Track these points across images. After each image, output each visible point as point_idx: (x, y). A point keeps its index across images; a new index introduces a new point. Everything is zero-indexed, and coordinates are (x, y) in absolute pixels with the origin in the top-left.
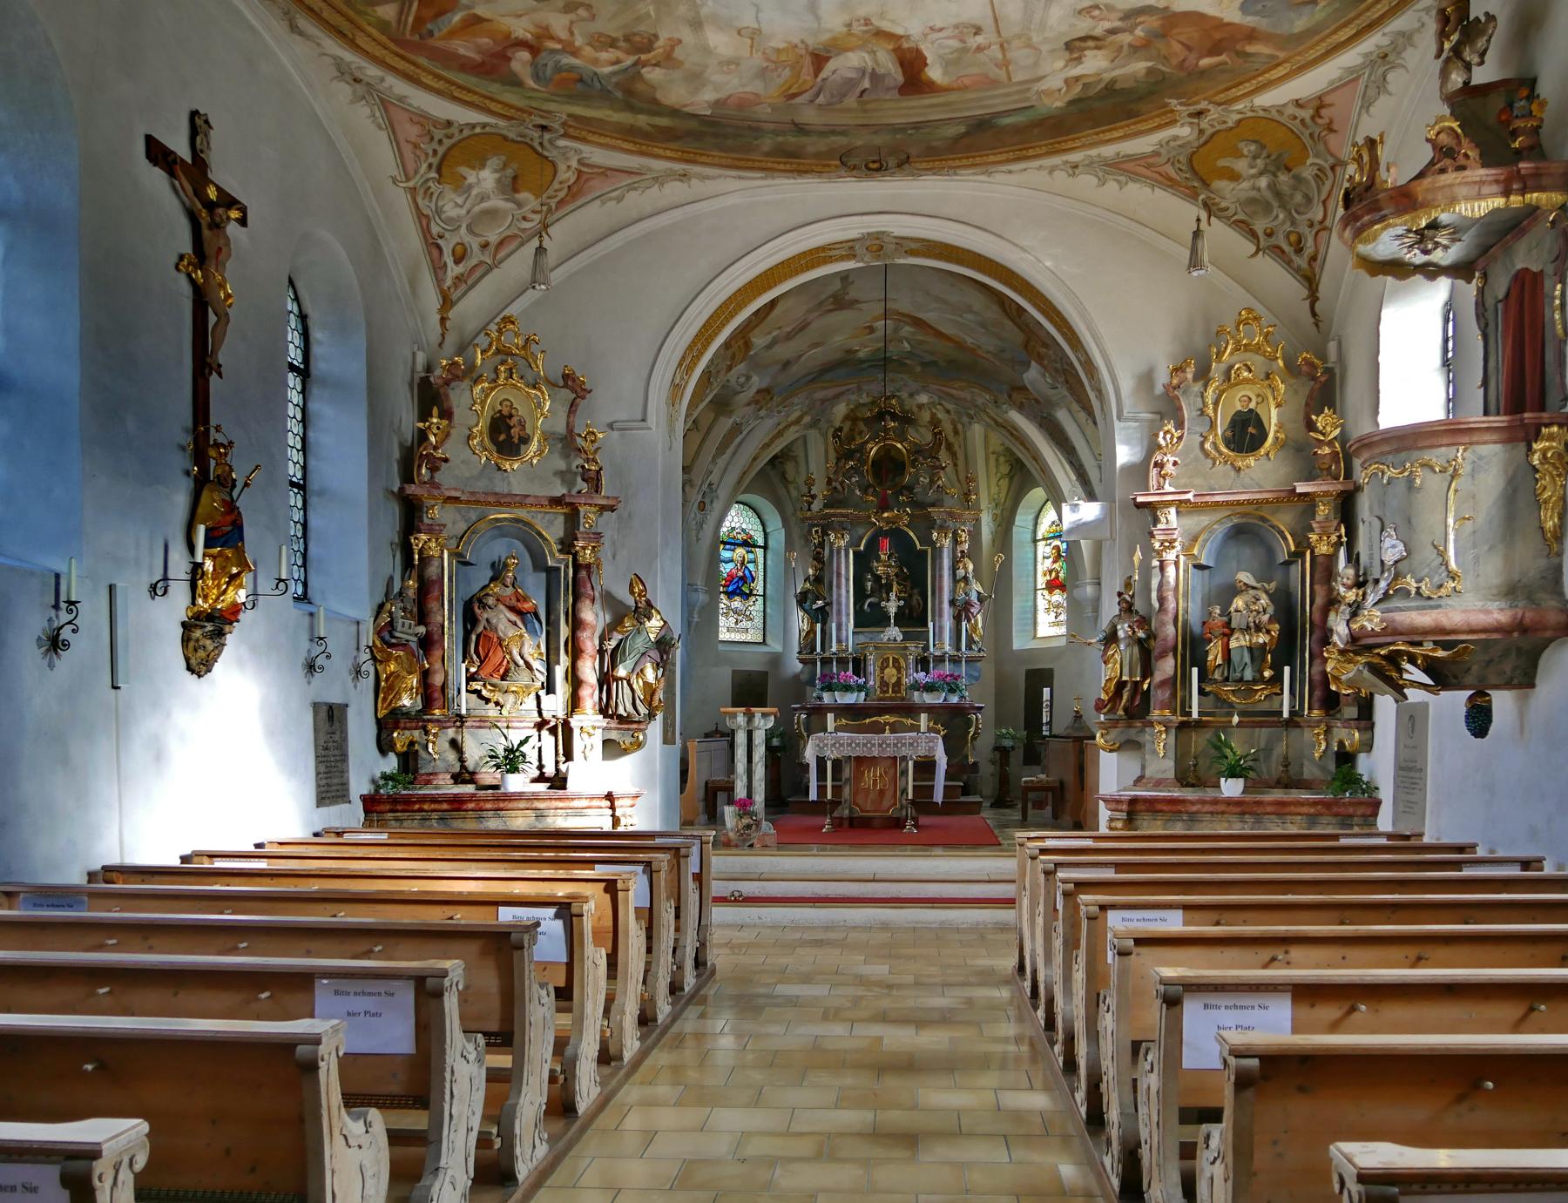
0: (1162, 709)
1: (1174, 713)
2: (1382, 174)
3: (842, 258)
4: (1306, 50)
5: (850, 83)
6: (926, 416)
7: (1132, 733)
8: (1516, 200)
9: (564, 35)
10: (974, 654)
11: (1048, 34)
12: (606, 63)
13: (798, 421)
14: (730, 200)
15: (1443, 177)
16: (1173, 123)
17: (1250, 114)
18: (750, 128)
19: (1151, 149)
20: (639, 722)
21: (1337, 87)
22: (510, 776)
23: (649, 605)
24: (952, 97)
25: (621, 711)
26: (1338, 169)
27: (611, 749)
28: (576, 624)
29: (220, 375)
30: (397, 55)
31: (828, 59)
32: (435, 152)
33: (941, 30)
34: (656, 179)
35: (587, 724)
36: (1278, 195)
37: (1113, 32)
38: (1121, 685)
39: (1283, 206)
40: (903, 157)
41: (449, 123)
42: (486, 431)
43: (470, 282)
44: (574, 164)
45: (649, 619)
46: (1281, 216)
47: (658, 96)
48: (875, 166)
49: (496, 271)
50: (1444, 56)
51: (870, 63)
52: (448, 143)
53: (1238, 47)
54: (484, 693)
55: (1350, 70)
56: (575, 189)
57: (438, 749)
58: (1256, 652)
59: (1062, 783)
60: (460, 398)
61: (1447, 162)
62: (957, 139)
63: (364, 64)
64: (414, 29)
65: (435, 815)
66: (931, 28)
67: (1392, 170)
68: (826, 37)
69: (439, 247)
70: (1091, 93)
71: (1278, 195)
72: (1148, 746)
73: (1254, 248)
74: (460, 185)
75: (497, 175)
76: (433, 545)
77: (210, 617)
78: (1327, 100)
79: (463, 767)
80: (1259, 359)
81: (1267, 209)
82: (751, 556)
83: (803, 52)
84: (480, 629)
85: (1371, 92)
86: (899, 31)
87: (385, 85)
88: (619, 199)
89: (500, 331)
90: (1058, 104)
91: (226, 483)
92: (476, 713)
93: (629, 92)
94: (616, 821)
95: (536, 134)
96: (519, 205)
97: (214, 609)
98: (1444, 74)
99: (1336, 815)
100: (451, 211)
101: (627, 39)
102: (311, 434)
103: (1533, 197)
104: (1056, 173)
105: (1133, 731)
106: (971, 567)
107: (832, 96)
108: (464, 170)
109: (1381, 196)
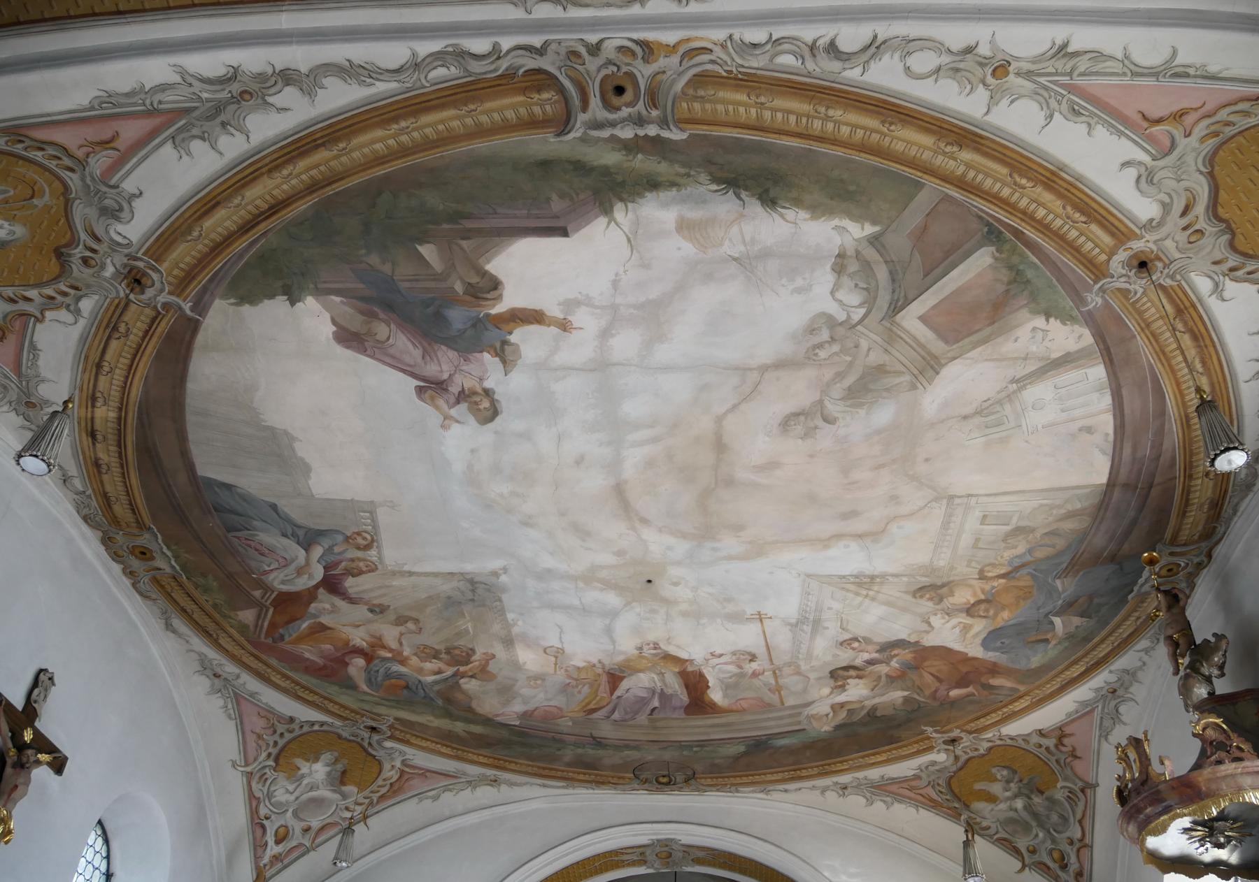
2: (1156, 767)
3: (633, 864)
4: (1043, 685)
5: (643, 701)
9: (394, 645)
11: (814, 663)
12: (430, 672)
14: (534, 805)
15: (1222, 767)
16: (929, 749)
17: (999, 742)
18: (554, 739)
19: (913, 772)
21: (1074, 718)
24: (732, 718)
26: (1088, 791)
30: (252, 655)
31: (622, 679)
32: (276, 743)
33: (721, 655)
34: (469, 782)
36: (1035, 815)
37: (871, 662)
39: (1041, 825)
40: (690, 773)
41: (292, 720)
43: (286, 861)
44: (398, 764)
46: (1041, 835)
47: (474, 705)
48: (665, 780)
49: (312, 853)
50: (1182, 673)
51: (659, 684)
52: (288, 736)
53: (983, 680)
55: (1084, 704)
56: (396, 787)
61: (1223, 754)
62: (737, 758)
63: (224, 661)
64: (267, 636)
66: (712, 654)
67: (1167, 762)
68: (620, 658)
69: (263, 827)
70: (856, 718)
71: (1035, 815)
73: (1019, 865)
74: (293, 774)
75: (328, 769)
78: (1067, 730)
81: (1027, 828)
83: (600, 671)
85: (1107, 723)
86: (684, 655)
87: (241, 681)
88: (435, 798)
90: (826, 728)
93: (449, 700)
95: (366, 734)
96: (344, 796)
98: (1185, 690)
100: (281, 796)
101: (448, 651)
104: (828, 793)
107: (626, 713)
108: (299, 762)
109: (1161, 787)
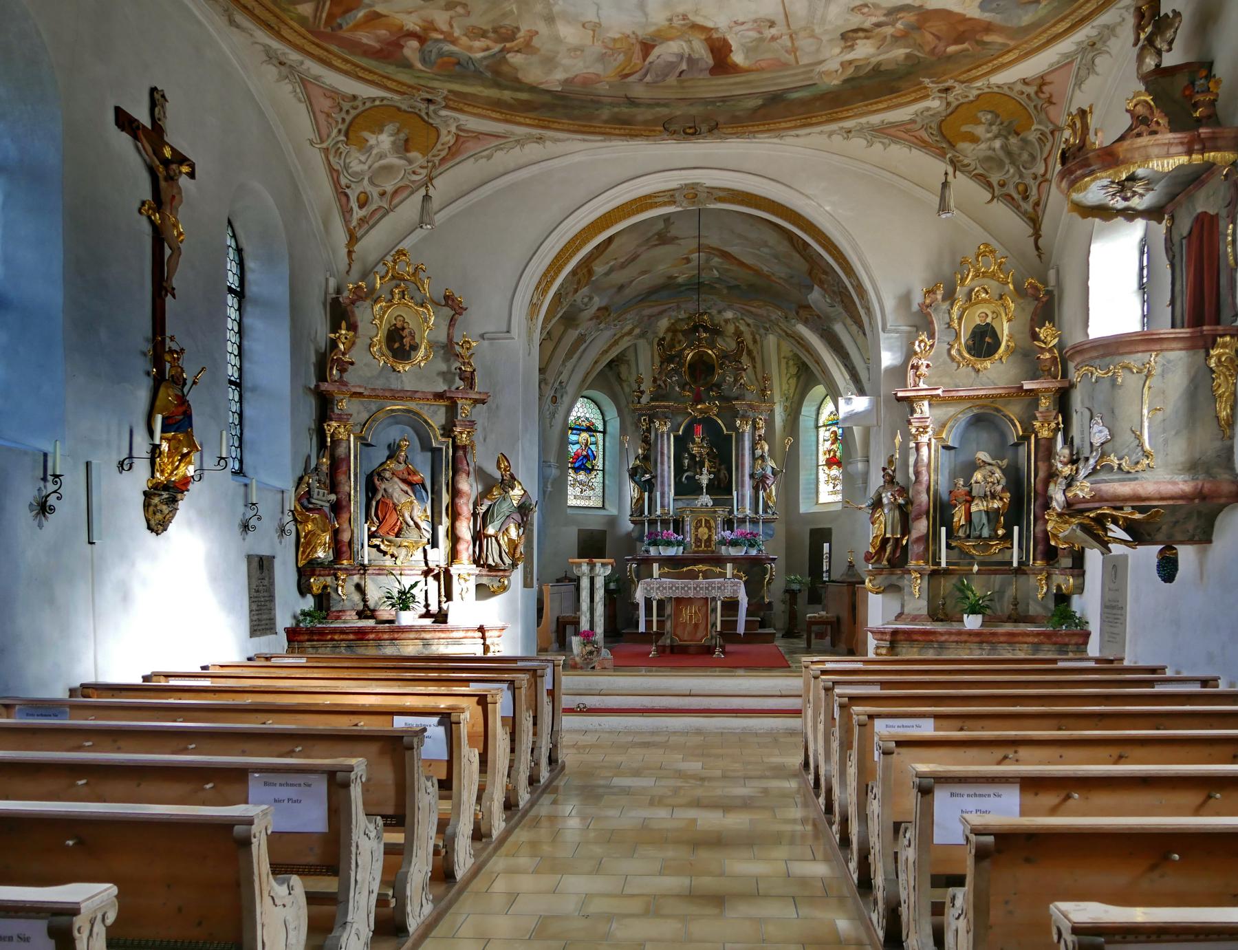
0: (917, 560)
1: (927, 563)
2: (1091, 137)
3: (665, 204)
4: (1031, 40)
5: (671, 66)
6: (731, 329)
7: (894, 579)
8: (1197, 158)
9: (445, 28)
10: (769, 516)
11: (828, 27)
12: (479, 50)
13: (630, 333)
14: (577, 158)
15: (1139, 140)
16: (926, 97)
17: (987, 90)
18: (592, 101)
19: (909, 117)
20: (505, 570)
21: (1055, 69)
22: (403, 613)
23: (513, 477)
24: (752, 77)
25: (490, 561)
26: (1057, 134)
27: (483, 591)
28: (455, 493)
29: (174, 296)
30: (314, 43)
31: (653, 47)
32: (343, 120)
33: (743, 23)
34: (518, 141)
35: (463, 572)
36: (1009, 154)
37: (878, 25)
38: (885, 541)
39: (1013, 163)
40: (713, 124)
41: (355, 98)
42: (383, 340)
43: (371, 223)
44: (453, 129)
45: (513, 489)
46: (1012, 171)
47: (520, 76)
48: (691, 131)
49: (391, 214)
50: (1140, 44)
51: (687, 50)
52: (353, 113)
53: (978, 37)
54: (382, 547)
55: (1066, 55)
56: (454, 149)
57: (346, 592)
58: (992, 515)
59: (838, 619)
60: (364, 314)
62: (756, 110)
63: (287, 51)
64: (327, 23)
65: (343, 644)
66: (735, 22)
67: (1099, 134)
68: (652, 29)
69: (346, 195)
70: (862, 73)
71: (1009, 154)
72: (906, 589)
73: (990, 196)
75: (392, 139)
76: (342, 430)
77: (166, 487)
78: (1048, 79)
79: (366, 606)
80: (994, 283)
81: (1001, 165)
82: (593, 439)
83: (634, 41)
84: (379, 497)
85: (1083, 73)
86: (710, 25)
87: (304, 67)
88: (489, 157)
89: (394, 261)
90: (836, 82)
91: (178, 381)
92: (376, 563)
93: (497, 73)
94: (486, 648)
95: (423, 106)
96: (410, 162)
97: (169, 481)
98: (1140, 59)
99: (1055, 644)
100: (356, 167)
101: (495, 31)
102: (245, 343)
103: (1211, 156)
104: (834, 137)
105: (894, 578)
106: (766, 448)
107: (657, 76)
108: (366, 134)
109: (1091, 155)
